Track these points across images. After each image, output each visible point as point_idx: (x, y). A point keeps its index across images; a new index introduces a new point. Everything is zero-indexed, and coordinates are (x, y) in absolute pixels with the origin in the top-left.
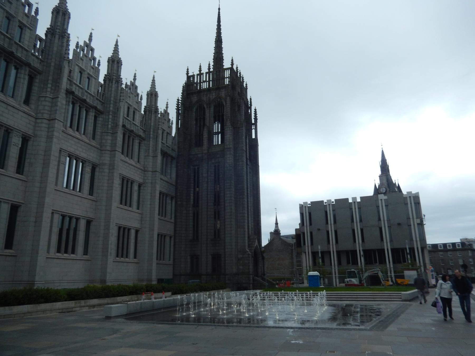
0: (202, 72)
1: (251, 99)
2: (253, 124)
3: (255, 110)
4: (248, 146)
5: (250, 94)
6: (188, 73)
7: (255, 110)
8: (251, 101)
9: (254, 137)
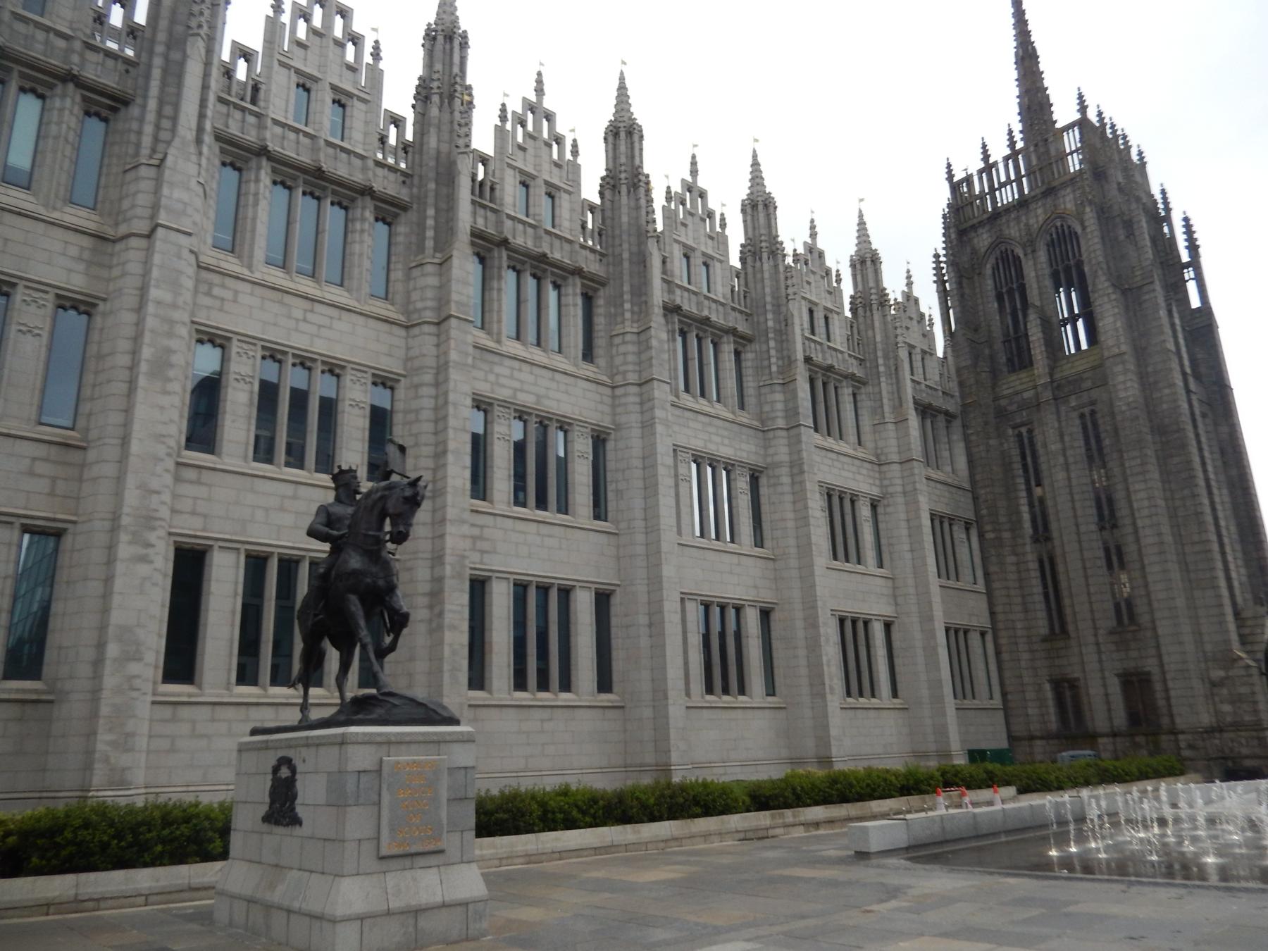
0: (991, 160)
1: (1163, 192)
2: (1187, 265)
3: (1186, 220)
6: (950, 176)
7: (1186, 220)
8: (1165, 199)
9: (1195, 302)
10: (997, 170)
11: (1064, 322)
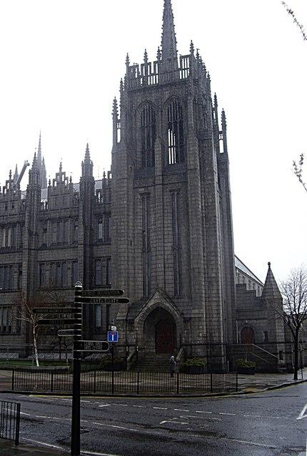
0: (148, 62)
1: (215, 96)
2: (221, 133)
3: (223, 112)
4: (218, 213)
5: (214, 88)
6: (128, 63)
7: (223, 112)
8: (216, 99)
9: (222, 151)
10: (150, 67)
11: (173, 146)
